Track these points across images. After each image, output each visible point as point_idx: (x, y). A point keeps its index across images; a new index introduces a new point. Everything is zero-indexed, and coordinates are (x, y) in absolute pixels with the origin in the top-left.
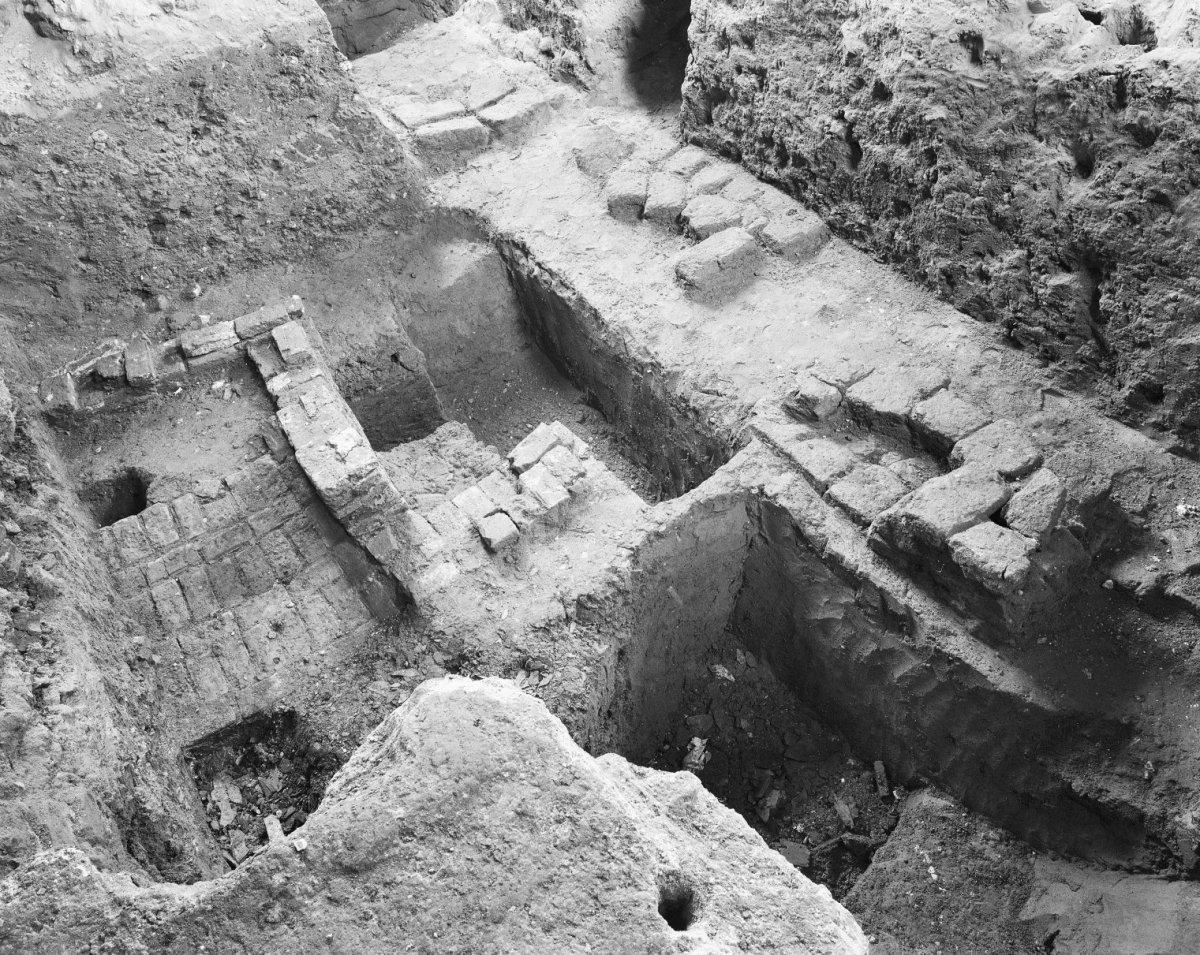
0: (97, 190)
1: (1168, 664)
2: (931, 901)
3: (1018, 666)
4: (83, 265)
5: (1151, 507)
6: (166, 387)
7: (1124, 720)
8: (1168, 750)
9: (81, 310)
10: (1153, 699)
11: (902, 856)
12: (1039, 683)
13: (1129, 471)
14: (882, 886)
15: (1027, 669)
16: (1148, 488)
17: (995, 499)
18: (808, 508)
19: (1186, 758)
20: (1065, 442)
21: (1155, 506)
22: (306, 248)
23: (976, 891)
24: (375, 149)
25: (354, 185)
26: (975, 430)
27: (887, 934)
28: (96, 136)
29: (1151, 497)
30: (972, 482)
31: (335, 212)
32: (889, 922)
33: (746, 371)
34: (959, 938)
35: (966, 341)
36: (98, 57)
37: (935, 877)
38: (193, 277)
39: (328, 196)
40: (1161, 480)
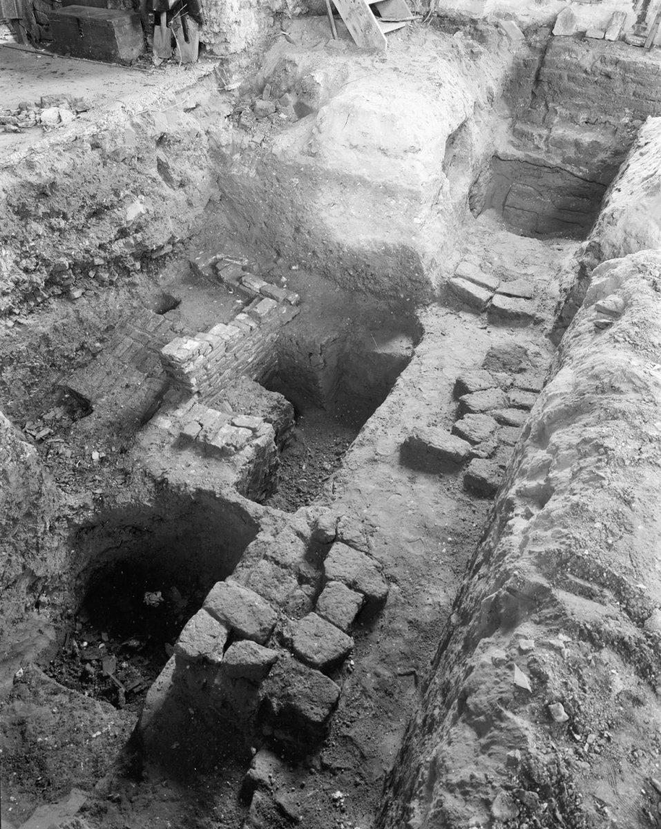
0: (283, 201)
1: (202, 804)
2: (80, 737)
3: (167, 699)
4: (263, 225)
5: (334, 772)
6: (229, 287)
7: (144, 774)
8: (128, 805)
9: (253, 241)
10: (167, 793)
11: (105, 716)
12: (158, 715)
13: (358, 748)
14: (85, 708)
15: (165, 704)
16: (348, 765)
17: (244, 629)
18: (252, 557)
19: (125, 818)
20: (370, 697)
21: (335, 775)
22: (351, 286)
23: (89, 761)
24: (409, 268)
25: (387, 276)
26: (330, 621)
27: (58, 718)
28: (294, 180)
29: (339, 769)
30: (254, 613)
31: (372, 281)
32: (65, 717)
33: (356, 496)
34: (60, 758)
35: (438, 608)
36: (313, 151)
37: (94, 736)
38: (298, 261)
39: (373, 272)
40: (359, 774)
